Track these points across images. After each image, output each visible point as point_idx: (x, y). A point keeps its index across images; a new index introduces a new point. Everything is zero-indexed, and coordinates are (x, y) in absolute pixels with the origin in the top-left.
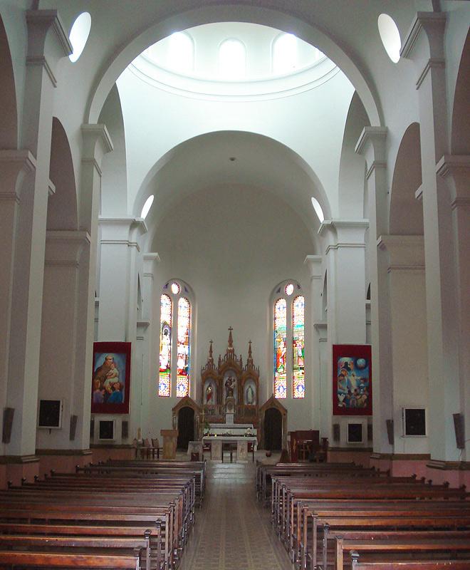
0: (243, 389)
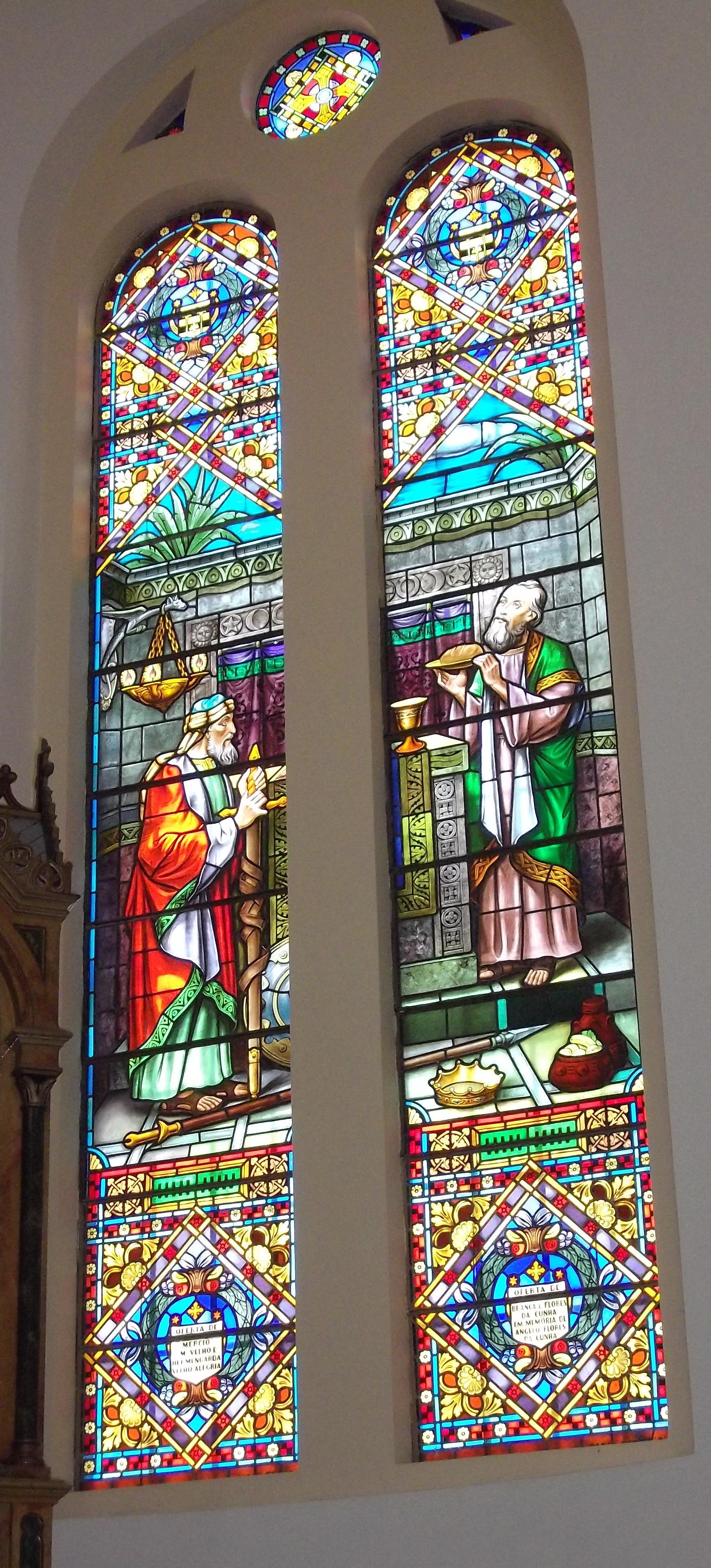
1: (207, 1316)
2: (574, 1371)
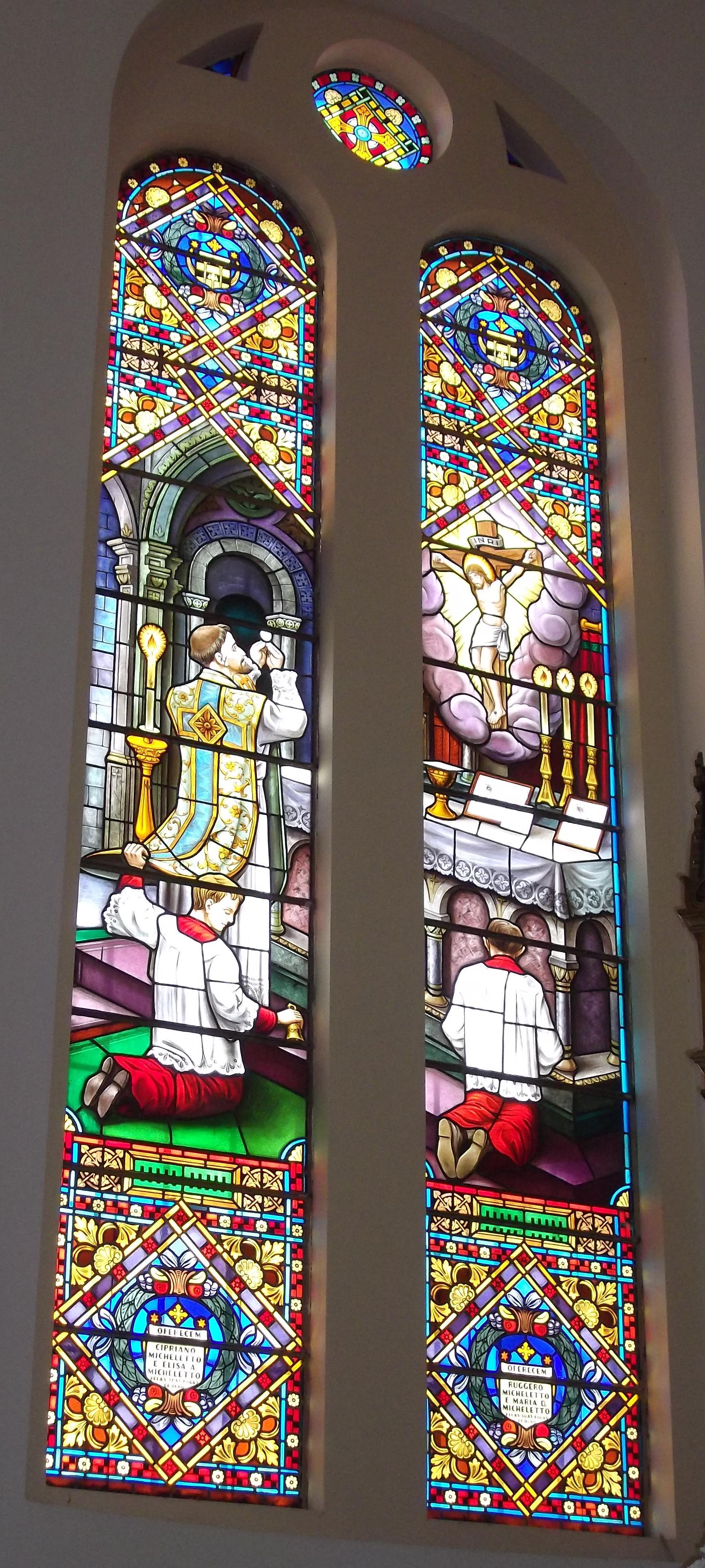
1: (190, 1322)
2: (202, 1424)
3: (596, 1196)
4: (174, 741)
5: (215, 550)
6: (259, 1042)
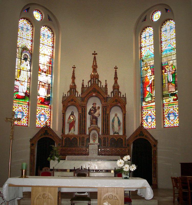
0: (108, 118)
3: (48, 105)
4: (21, 70)
5: (24, 54)
6: (26, 93)
